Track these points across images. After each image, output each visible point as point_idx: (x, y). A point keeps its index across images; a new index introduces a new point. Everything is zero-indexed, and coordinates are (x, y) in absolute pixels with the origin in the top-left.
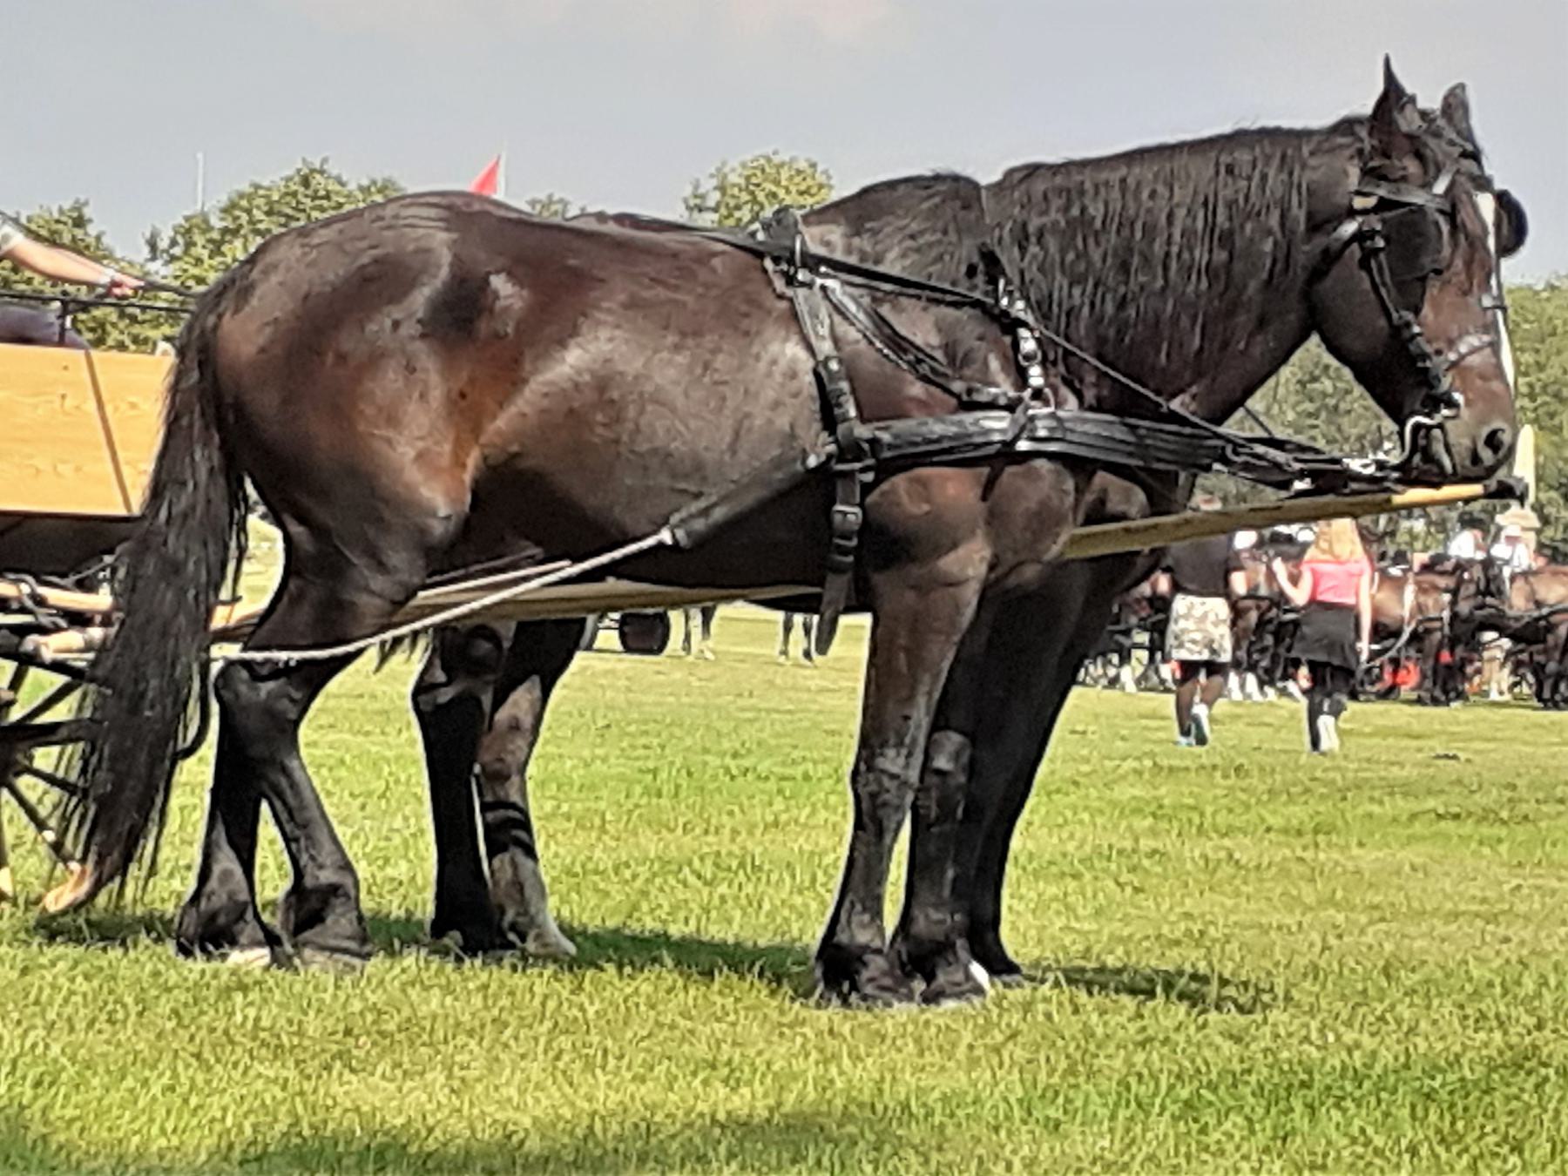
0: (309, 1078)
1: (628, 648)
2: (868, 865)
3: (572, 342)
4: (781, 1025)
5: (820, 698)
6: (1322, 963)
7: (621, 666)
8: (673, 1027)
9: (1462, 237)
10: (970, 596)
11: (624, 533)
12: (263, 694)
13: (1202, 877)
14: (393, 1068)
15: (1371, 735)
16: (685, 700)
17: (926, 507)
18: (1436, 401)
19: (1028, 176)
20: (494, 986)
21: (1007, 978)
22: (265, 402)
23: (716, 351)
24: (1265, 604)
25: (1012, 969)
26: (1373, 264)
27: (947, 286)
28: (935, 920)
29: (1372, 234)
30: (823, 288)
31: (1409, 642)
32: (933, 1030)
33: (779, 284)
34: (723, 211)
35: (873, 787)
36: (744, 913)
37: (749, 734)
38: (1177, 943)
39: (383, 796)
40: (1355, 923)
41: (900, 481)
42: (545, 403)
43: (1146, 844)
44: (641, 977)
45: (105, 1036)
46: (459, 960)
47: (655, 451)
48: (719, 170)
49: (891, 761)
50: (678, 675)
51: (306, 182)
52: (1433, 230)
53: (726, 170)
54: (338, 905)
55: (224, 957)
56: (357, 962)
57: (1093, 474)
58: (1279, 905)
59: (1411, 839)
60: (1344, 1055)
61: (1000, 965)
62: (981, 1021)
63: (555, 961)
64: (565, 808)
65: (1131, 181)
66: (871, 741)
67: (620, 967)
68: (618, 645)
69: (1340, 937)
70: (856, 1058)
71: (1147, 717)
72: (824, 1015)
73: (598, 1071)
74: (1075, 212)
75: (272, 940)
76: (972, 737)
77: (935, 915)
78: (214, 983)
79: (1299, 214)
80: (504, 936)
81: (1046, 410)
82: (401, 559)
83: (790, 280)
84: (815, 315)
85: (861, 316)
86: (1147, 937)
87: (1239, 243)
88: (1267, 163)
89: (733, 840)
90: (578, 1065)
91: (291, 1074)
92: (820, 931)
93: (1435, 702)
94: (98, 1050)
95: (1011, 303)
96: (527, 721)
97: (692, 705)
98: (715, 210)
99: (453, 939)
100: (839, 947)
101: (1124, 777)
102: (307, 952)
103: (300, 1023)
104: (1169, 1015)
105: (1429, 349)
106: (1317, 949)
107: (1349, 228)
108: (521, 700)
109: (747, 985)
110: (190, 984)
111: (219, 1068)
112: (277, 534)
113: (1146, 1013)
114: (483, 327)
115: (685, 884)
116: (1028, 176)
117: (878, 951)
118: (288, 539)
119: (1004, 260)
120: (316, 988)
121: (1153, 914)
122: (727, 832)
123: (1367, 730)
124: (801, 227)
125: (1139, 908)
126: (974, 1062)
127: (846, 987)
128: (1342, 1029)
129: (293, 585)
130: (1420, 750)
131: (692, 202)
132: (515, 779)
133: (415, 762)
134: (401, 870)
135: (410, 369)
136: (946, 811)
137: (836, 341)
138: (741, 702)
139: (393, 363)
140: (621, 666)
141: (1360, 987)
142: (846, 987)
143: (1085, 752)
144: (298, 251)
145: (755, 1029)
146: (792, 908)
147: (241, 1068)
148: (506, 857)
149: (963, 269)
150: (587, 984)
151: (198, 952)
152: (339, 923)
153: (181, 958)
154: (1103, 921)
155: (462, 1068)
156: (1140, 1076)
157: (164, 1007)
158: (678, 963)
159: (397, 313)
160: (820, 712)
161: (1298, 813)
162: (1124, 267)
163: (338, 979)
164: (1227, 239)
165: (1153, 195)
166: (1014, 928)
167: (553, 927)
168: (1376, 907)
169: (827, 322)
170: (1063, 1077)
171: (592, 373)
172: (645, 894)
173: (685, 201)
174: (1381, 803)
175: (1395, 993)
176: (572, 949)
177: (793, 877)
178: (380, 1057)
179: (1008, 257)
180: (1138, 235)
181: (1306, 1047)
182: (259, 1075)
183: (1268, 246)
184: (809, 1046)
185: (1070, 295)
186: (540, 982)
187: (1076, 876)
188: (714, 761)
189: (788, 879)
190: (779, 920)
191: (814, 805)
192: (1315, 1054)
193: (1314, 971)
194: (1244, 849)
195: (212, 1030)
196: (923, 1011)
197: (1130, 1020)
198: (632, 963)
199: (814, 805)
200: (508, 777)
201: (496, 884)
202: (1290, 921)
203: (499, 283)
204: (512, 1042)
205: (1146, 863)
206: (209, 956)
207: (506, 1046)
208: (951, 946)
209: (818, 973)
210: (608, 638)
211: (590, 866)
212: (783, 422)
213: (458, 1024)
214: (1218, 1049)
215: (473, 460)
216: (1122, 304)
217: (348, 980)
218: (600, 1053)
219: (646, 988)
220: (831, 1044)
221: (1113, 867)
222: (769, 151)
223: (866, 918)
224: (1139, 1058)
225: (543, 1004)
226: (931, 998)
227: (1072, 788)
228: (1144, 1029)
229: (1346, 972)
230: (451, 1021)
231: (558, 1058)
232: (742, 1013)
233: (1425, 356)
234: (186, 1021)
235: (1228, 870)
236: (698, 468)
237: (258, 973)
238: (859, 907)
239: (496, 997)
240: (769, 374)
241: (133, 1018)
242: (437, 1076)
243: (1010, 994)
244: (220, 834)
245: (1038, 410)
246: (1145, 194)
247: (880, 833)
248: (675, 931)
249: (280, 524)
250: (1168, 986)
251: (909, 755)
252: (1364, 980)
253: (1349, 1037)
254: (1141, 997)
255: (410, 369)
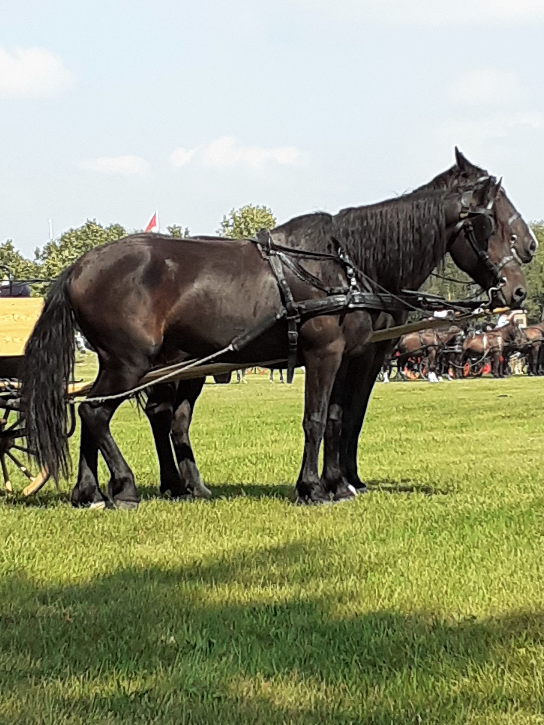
0: (123, 547)
1: (217, 382)
2: (311, 454)
3: (196, 281)
4: (286, 513)
5: (285, 394)
6: (469, 474)
7: (215, 389)
8: (248, 517)
9: (498, 223)
10: (339, 358)
11: (216, 346)
12: (96, 412)
13: (424, 447)
14: (152, 541)
15: (476, 390)
16: (239, 399)
17: (321, 329)
18: (497, 281)
19: (348, 212)
20: (184, 508)
21: (361, 489)
22: (89, 309)
23: (245, 280)
24: (437, 348)
25: (363, 485)
26: (470, 236)
27: (321, 253)
28: (335, 472)
29: (468, 226)
30: (279, 256)
31: (487, 356)
32: (338, 510)
33: (264, 255)
34: (235, 226)
35: (311, 427)
36: (268, 474)
37: (264, 409)
38: (419, 471)
39: (138, 443)
40: (479, 459)
41: (312, 320)
42: (188, 302)
43: (404, 436)
44: (235, 500)
45: (50, 539)
46: (171, 499)
47: (228, 317)
48: (232, 212)
49: (316, 417)
50: (236, 390)
51: (88, 226)
52: (488, 221)
53: (235, 211)
54: (127, 484)
55: (89, 506)
56: (135, 504)
57: (379, 313)
58: (452, 454)
59: (494, 427)
60: (480, 506)
61: (359, 485)
62: (354, 505)
63: (205, 497)
64: (202, 441)
65: (384, 212)
66: (308, 412)
67: (227, 497)
68: (213, 381)
69: (474, 464)
70: (313, 523)
71: (398, 390)
72: (299, 508)
73: (224, 536)
74: (365, 224)
75: (105, 499)
76: (341, 406)
77: (334, 470)
78: (86, 516)
79: (442, 221)
80: (186, 490)
81: (358, 293)
82: (140, 360)
83: (268, 254)
84: (277, 265)
85: (292, 265)
86: (408, 470)
87: (423, 231)
88: (429, 204)
89: (261, 448)
90: (217, 533)
91: (117, 546)
92: (296, 479)
93: (495, 377)
94: (48, 544)
95: (344, 256)
96: (187, 413)
97: (241, 400)
98: (232, 226)
99: (168, 493)
100: (303, 483)
101: (393, 413)
102: (118, 502)
103: (118, 528)
104: (419, 497)
105: (492, 263)
106: (467, 470)
107: (460, 224)
108: (184, 407)
109: (272, 500)
110: (77, 517)
111: (91, 546)
112: (96, 354)
113: (411, 497)
114: (164, 278)
115: (247, 466)
116: (348, 212)
117: (317, 484)
118: (100, 357)
119: (340, 242)
120: (122, 515)
121: (409, 461)
122: (259, 445)
123: (475, 388)
124: (270, 235)
125: (404, 460)
126: (353, 521)
127: (307, 497)
128: (479, 497)
129: (104, 372)
130: (494, 394)
131: (224, 224)
132: (185, 434)
133: (147, 429)
134: (147, 469)
135: (139, 294)
136: (335, 431)
137: (284, 273)
138: (259, 398)
139: (134, 292)
140: (215, 389)
141: (483, 481)
142: (307, 497)
143: (379, 405)
144: (96, 256)
145: (277, 516)
146: (285, 470)
147: (99, 546)
148: (184, 462)
149: (327, 245)
150: (216, 504)
151: (80, 505)
152: (128, 491)
153: (73, 508)
154: (392, 466)
155: (176, 539)
156: (411, 520)
157: (70, 526)
158: (247, 494)
159: (131, 275)
160: (286, 399)
161: (454, 421)
162: (384, 243)
163: (130, 510)
164: (418, 230)
165: (391, 217)
166: (362, 470)
167: (202, 485)
168: (485, 452)
169: (281, 267)
170: (385, 523)
171: (203, 289)
172: (233, 470)
173: (222, 223)
174: (482, 414)
175: (495, 483)
176: (210, 492)
177: (284, 459)
178: (147, 537)
179: (342, 241)
180: (388, 231)
181: (466, 504)
182: (106, 548)
183: (433, 232)
184: (296, 520)
185: (365, 254)
186: (201, 505)
187: (382, 450)
188: (252, 420)
189: (282, 460)
190: (280, 475)
191: (288, 433)
192: (470, 506)
193: (467, 477)
194: (437, 435)
195: (87, 533)
196: (334, 504)
197: (405, 500)
198: (231, 496)
199: (288, 433)
200: (182, 434)
201: (182, 472)
202: (456, 460)
203: (168, 262)
204: (193, 528)
205: (405, 443)
206: (84, 507)
207: (191, 529)
208: (340, 479)
209: (297, 492)
210: (210, 379)
211: (213, 461)
212: (271, 303)
213: (173, 523)
214: (437, 507)
215: (163, 324)
216: (384, 256)
217: (133, 510)
218: (224, 529)
219: (237, 504)
220: (304, 518)
221: (394, 446)
222: (248, 204)
223: (312, 473)
224: (410, 513)
225: (202, 513)
226: (336, 499)
227: (376, 419)
228: (410, 503)
229: (478, 476)
230: (171, 522)
231: (209, 531)
232: (272, 510)
233: (492, 266)
234: (78, 531)
235: (433, 443)
236: (243, 322)
237: (101, 511)
238: (309, 469)
239: (185, 513)
240: (264, 287)
241: (59, 530)
242: (168, 542)
243: (363, 495)
244: (85, 463)
245: (356, 293)
246: (389, 216)
247: (315, 442)
248: (245, 482)
249: (96, 350)
250: (417, 488)
251: (322, 415)
252: (484, 479)
253: (482, 499)
254: (408, 492)
255: (139, 294)
